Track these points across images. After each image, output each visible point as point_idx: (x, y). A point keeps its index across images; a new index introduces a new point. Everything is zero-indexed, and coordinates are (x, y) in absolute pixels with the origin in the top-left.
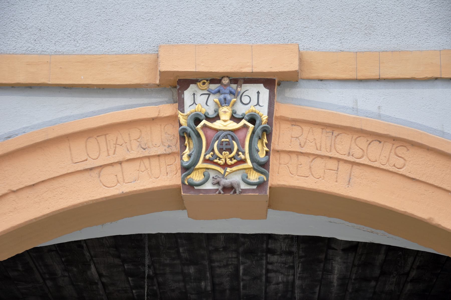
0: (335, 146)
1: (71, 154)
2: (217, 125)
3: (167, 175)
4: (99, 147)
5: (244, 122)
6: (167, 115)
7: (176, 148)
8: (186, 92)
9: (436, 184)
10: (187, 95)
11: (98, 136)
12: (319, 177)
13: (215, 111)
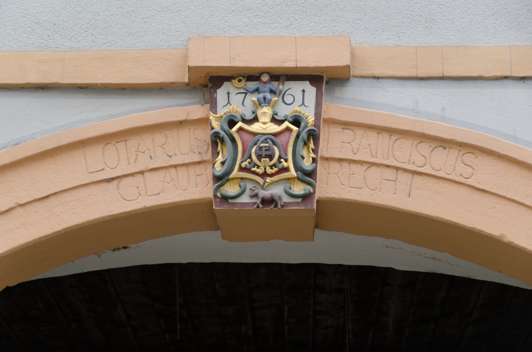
0: (393, 153)
1: (86, 163)
2: (255, 127)
3: (197, 186)
4: (119, 155)
5: (286, 124)
6: (197, 117)
7: (208, 156)
8: (219, 91)
9: (508, 196)
10: (221, 94)
11: (117, 142)
12: (374, 188)
13: (253, 113)
